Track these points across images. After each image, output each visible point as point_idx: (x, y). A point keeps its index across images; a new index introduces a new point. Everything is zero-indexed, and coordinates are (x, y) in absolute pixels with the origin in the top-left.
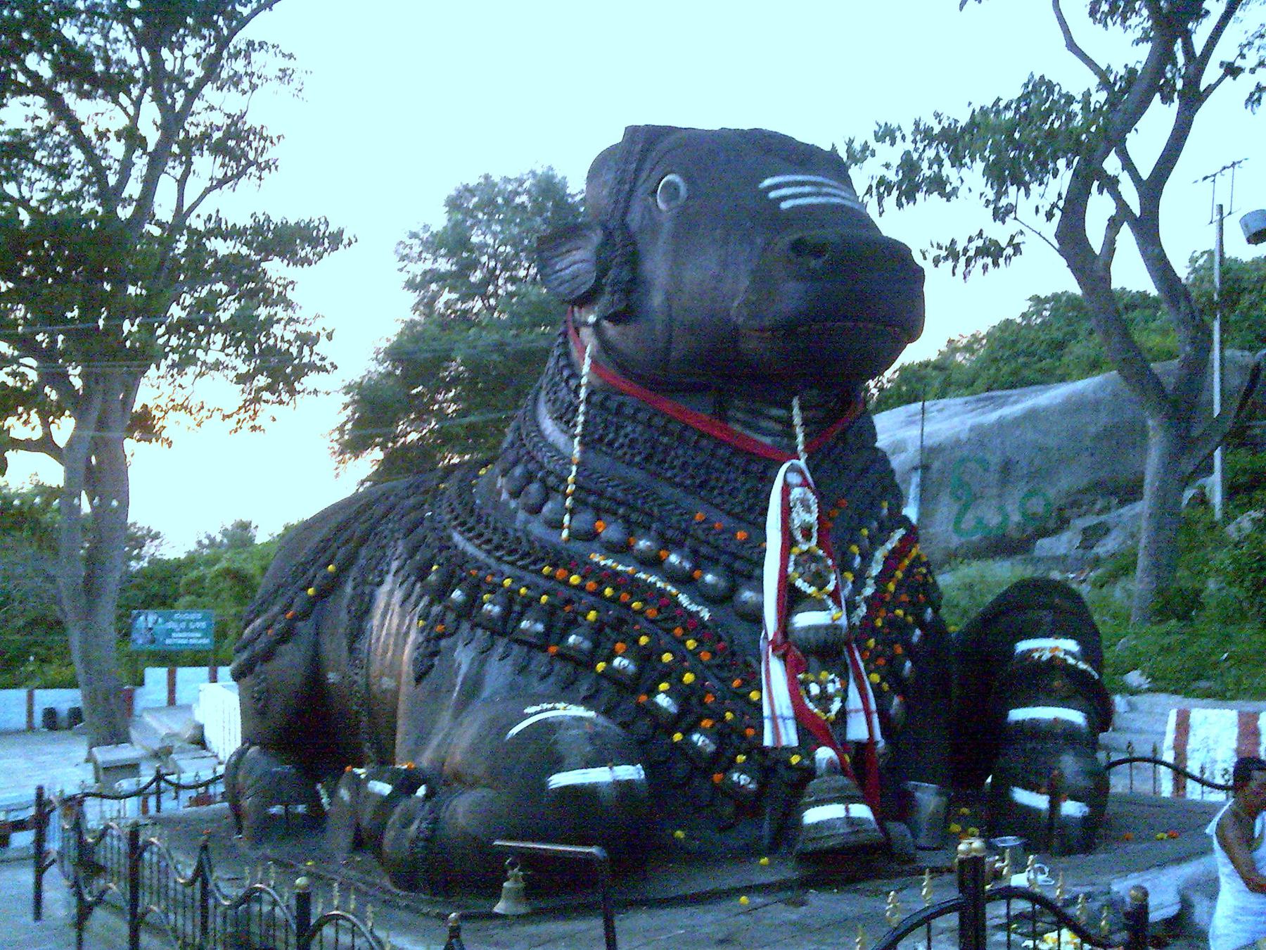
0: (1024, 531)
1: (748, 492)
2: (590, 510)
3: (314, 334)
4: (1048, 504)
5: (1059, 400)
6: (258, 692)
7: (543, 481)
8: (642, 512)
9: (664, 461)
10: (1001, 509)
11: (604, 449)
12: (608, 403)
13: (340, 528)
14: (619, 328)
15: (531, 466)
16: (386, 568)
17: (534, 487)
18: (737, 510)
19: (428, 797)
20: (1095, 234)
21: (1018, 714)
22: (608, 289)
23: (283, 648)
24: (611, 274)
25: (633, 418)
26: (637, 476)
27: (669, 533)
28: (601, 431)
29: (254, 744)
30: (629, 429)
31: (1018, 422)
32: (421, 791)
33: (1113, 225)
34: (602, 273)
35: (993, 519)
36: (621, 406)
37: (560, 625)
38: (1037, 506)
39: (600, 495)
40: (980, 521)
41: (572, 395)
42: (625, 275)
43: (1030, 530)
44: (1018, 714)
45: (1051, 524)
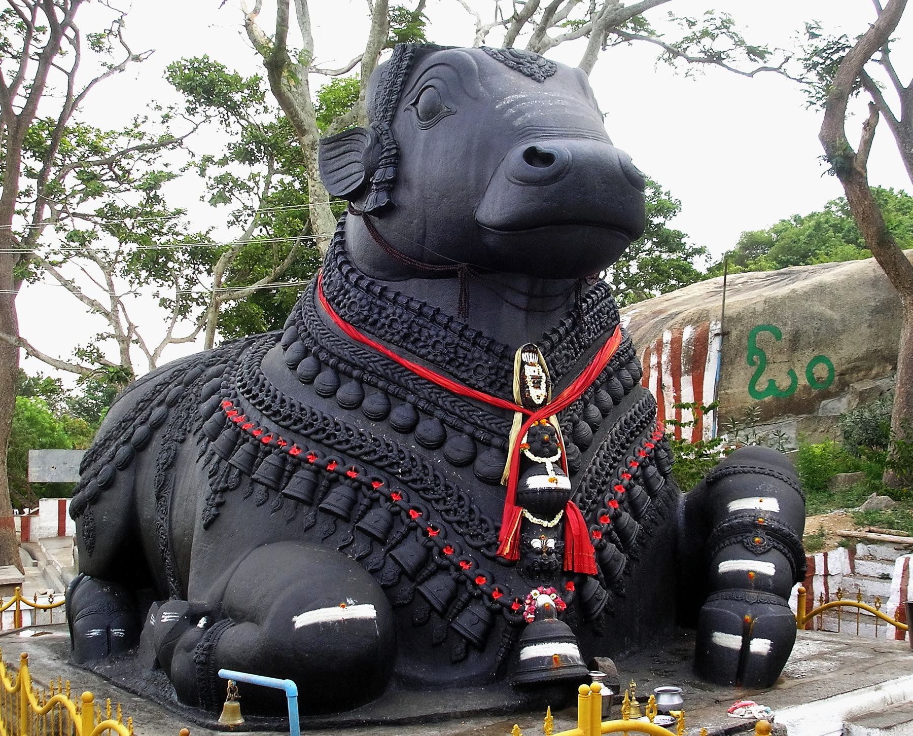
0: (810, 394)
1: (491, 368)
2: (354, 382)
3: (888, 190)
4: (831, 370)
5: (842, 277)
6: (88, 530)
7: (316, 356)
8: (399, 385)
9: (417, 340)
10: (791, 373)
11: (368, 328)
12: (372, 287)
13: (156, 392)
14: (382, 222)
15: (308, 342)
16: (188, 429)
17: (309, 361)
18: (481, 384)
19: (207, 626)
20: (854, 136)
21: (725, 566)
22: (374, 187)
23: (107, 493)
24: (378, 174)
25: (395, 301)
26: (392, 351)
27: (421, 404)
28: (365, 313)
29: (85, 574)
30: (390, 311)
31: (807, 295)
32: (202, 622)
33: (870, 127)
34: (370, 173)
35: (784, 383)
36: (384, 289)
37: (324, 482)
38: (821, 371)
39: (363, 369)
40: (772, 382)
41: (344, 280)
42: (390, 174)
43: (815, 392)
44: (725, 566)
45: (832, 388)
